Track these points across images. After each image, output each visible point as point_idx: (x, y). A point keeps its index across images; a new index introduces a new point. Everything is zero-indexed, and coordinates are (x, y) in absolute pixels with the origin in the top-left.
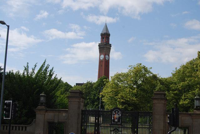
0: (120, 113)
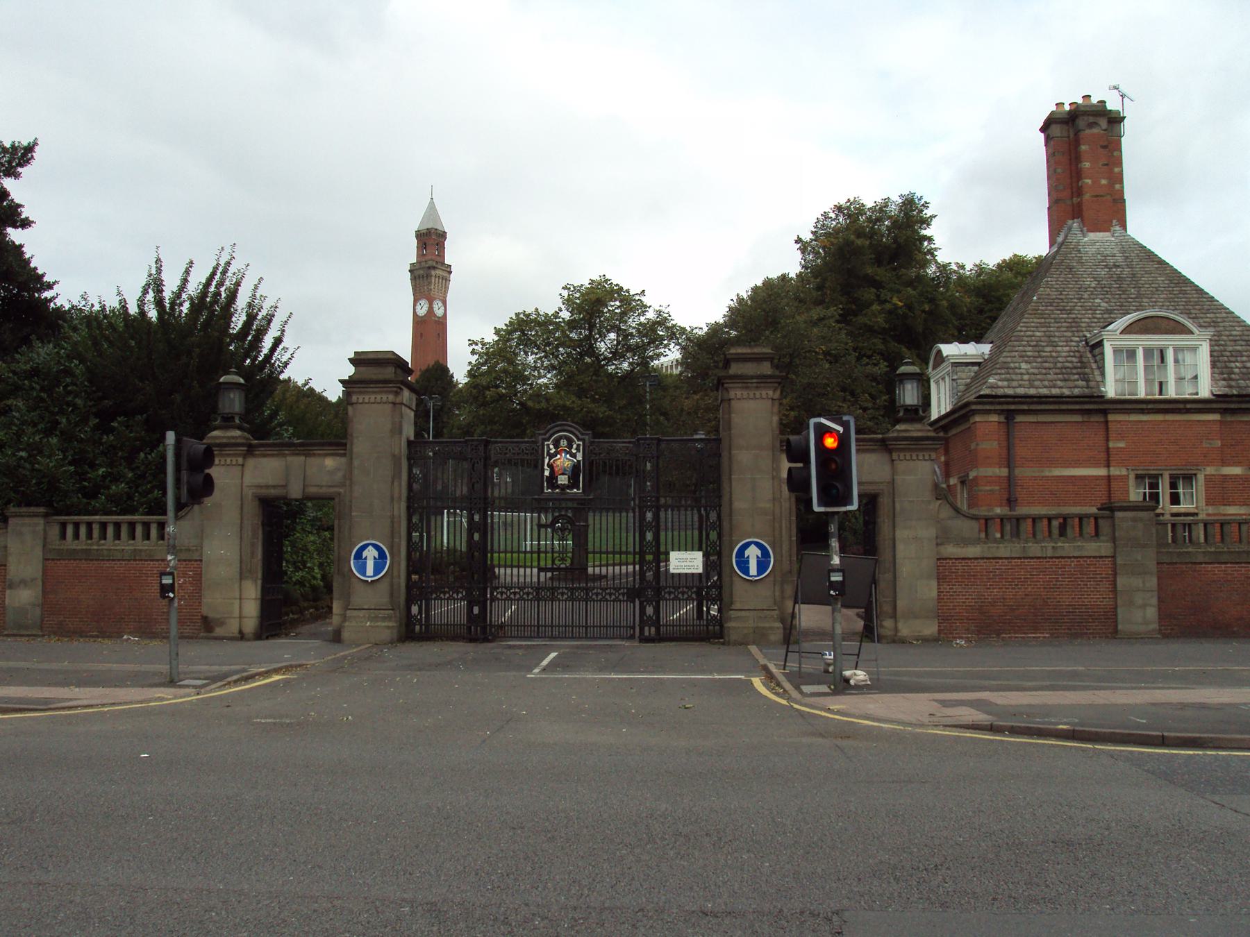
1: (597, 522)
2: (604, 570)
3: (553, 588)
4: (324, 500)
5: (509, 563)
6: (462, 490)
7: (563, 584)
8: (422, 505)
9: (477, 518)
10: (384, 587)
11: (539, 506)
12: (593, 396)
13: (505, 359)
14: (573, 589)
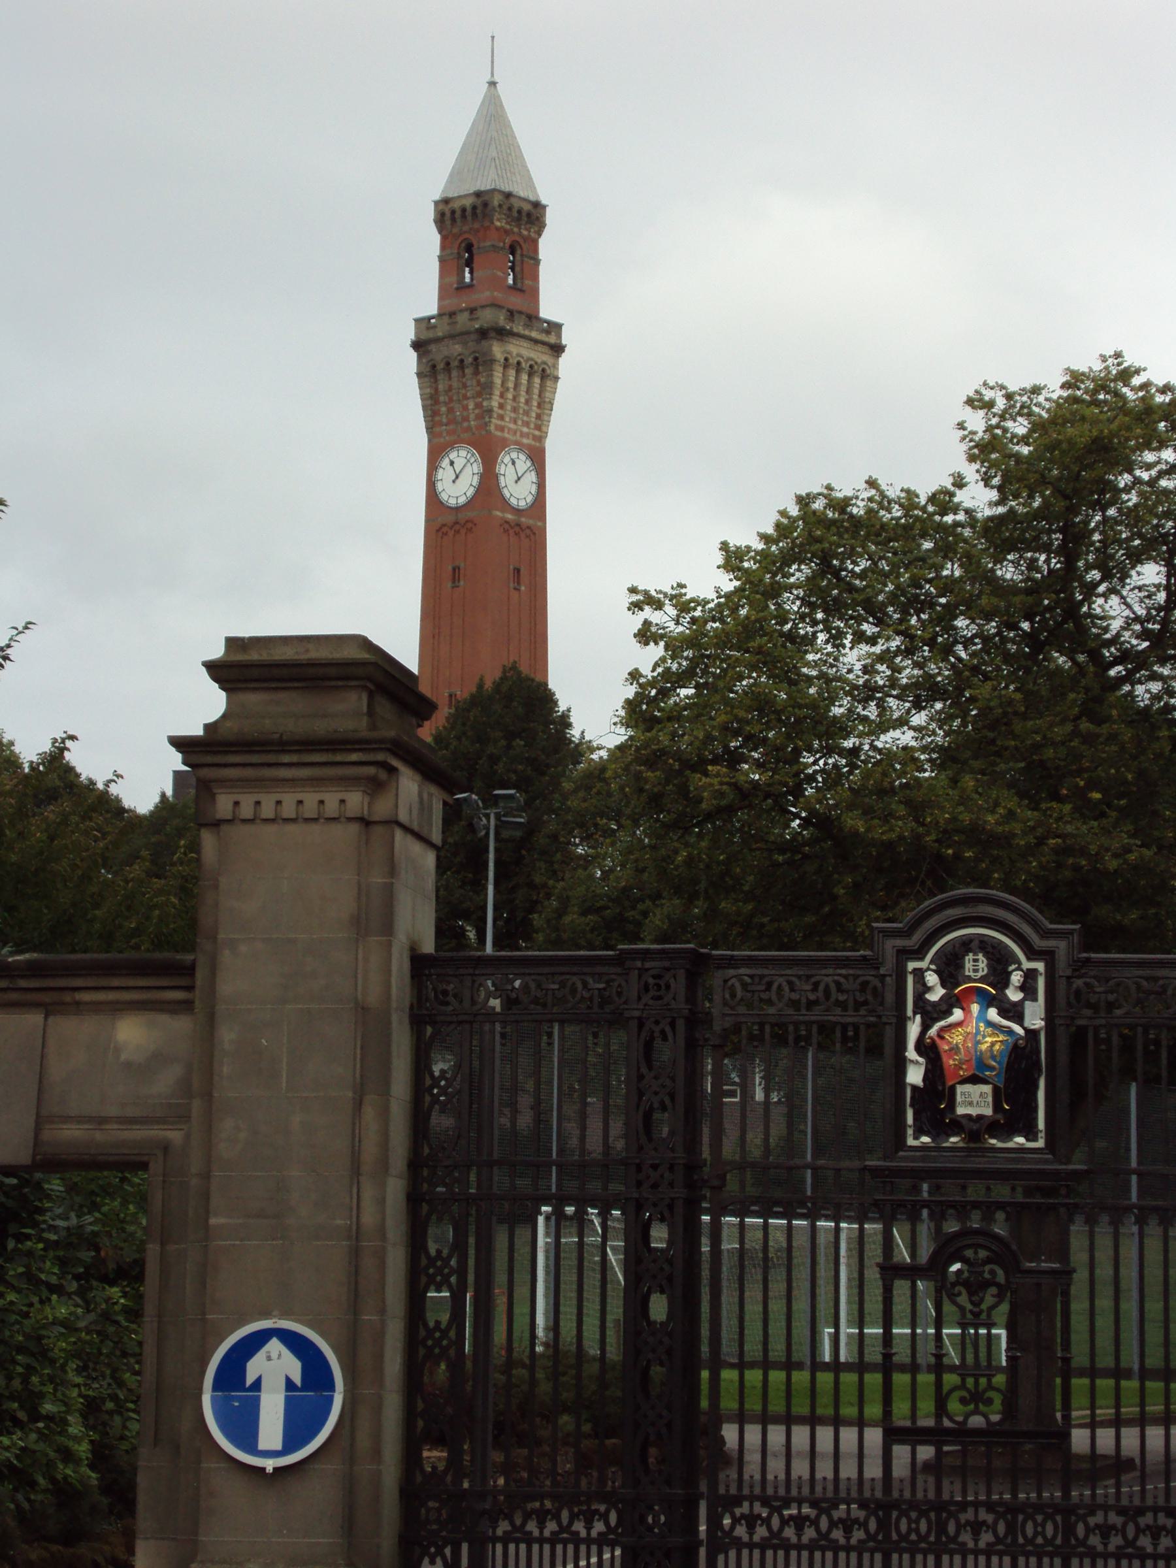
0: (1030, 975)
1: (1104, 1255)
2: (1130, 1437)
3: (940, 1506)
4: (109, 1172)
5: (777, 1406)
6: (601, 1132)
7: (977, 1492)
8: (461, 1188)
9: (659, 1237)
10: (319, 1496)
11: (884, 1193)
12: (1080, 795)
13: (766, 661)
14: (1011, 1511)
